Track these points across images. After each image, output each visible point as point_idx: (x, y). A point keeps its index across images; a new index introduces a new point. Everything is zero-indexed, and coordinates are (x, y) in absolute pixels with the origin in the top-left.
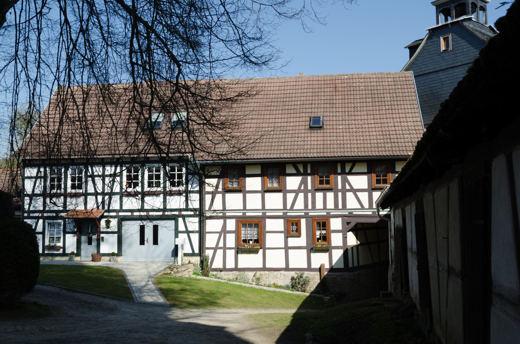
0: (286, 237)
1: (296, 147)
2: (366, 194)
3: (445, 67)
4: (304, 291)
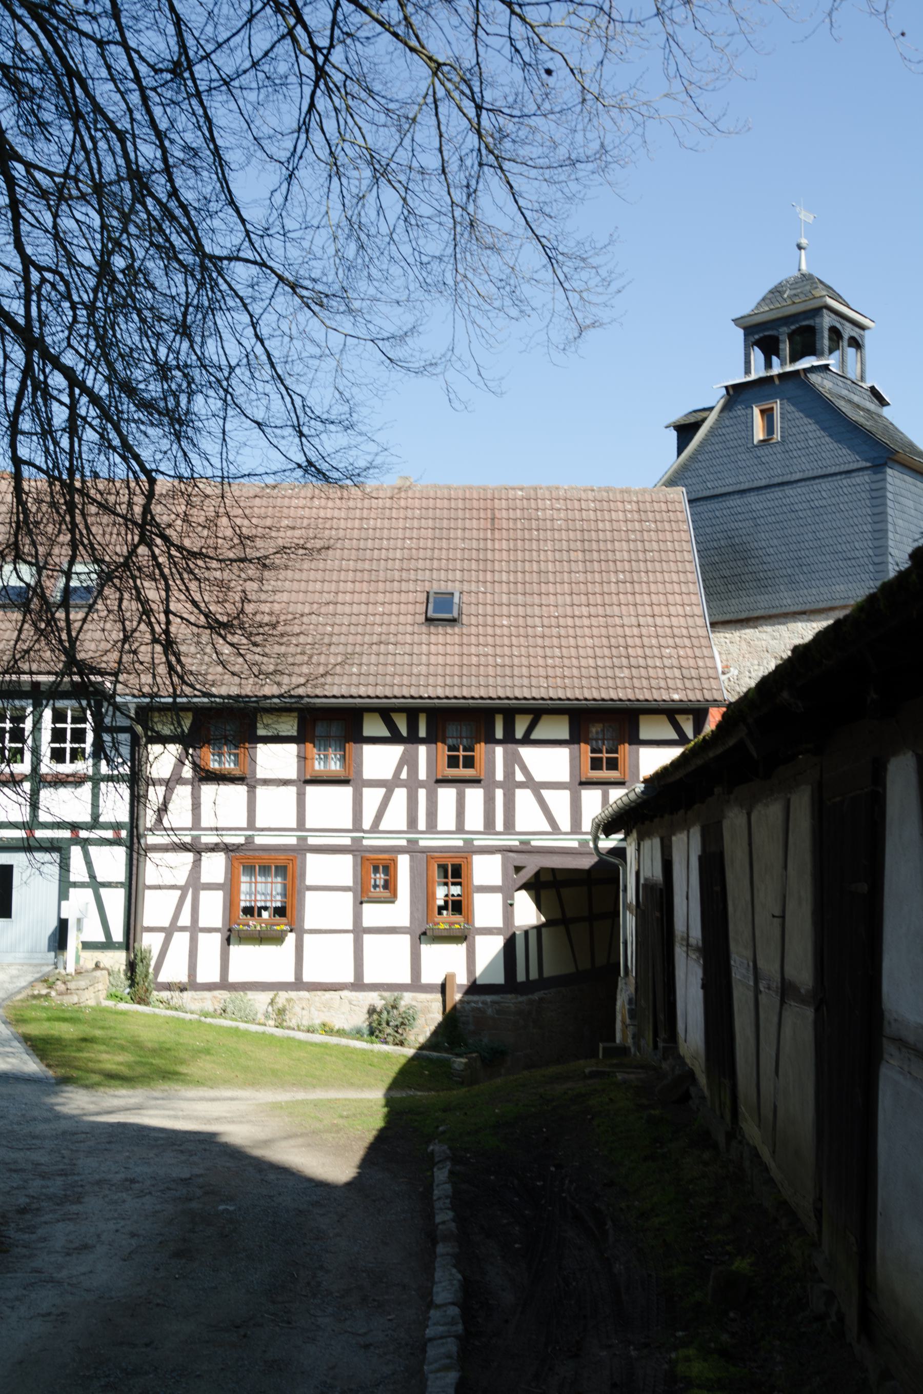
0: (359, 903)
1: (390, 669)
2: (566, 795)
3: (763, 483)
4: (401, 1044)
